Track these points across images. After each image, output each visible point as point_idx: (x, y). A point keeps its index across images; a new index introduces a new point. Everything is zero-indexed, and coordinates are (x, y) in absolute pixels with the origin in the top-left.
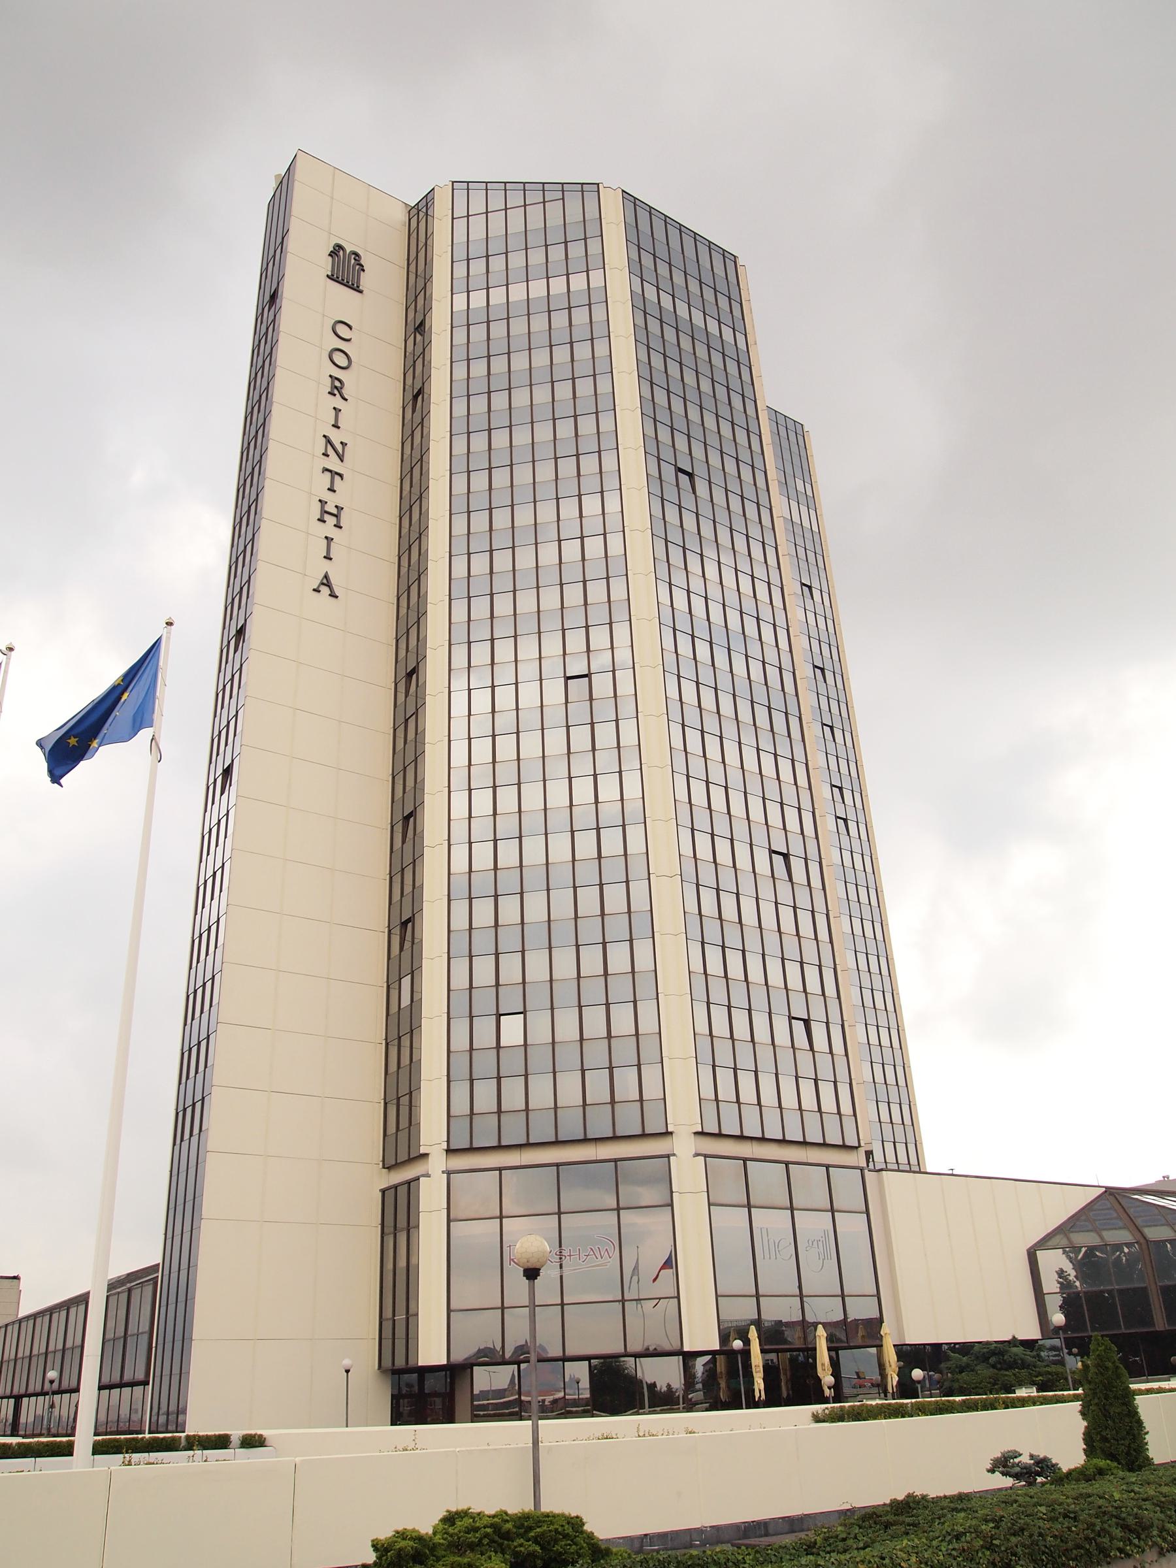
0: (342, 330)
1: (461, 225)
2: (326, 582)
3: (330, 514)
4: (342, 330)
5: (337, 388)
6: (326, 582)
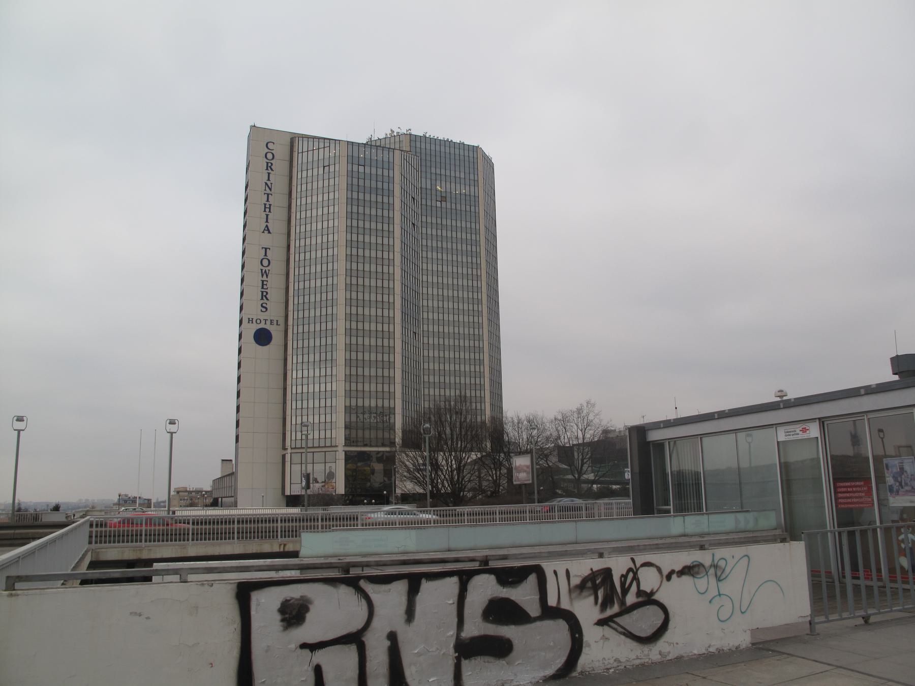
1: (300, 155)
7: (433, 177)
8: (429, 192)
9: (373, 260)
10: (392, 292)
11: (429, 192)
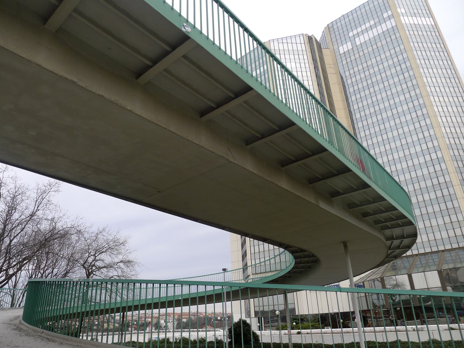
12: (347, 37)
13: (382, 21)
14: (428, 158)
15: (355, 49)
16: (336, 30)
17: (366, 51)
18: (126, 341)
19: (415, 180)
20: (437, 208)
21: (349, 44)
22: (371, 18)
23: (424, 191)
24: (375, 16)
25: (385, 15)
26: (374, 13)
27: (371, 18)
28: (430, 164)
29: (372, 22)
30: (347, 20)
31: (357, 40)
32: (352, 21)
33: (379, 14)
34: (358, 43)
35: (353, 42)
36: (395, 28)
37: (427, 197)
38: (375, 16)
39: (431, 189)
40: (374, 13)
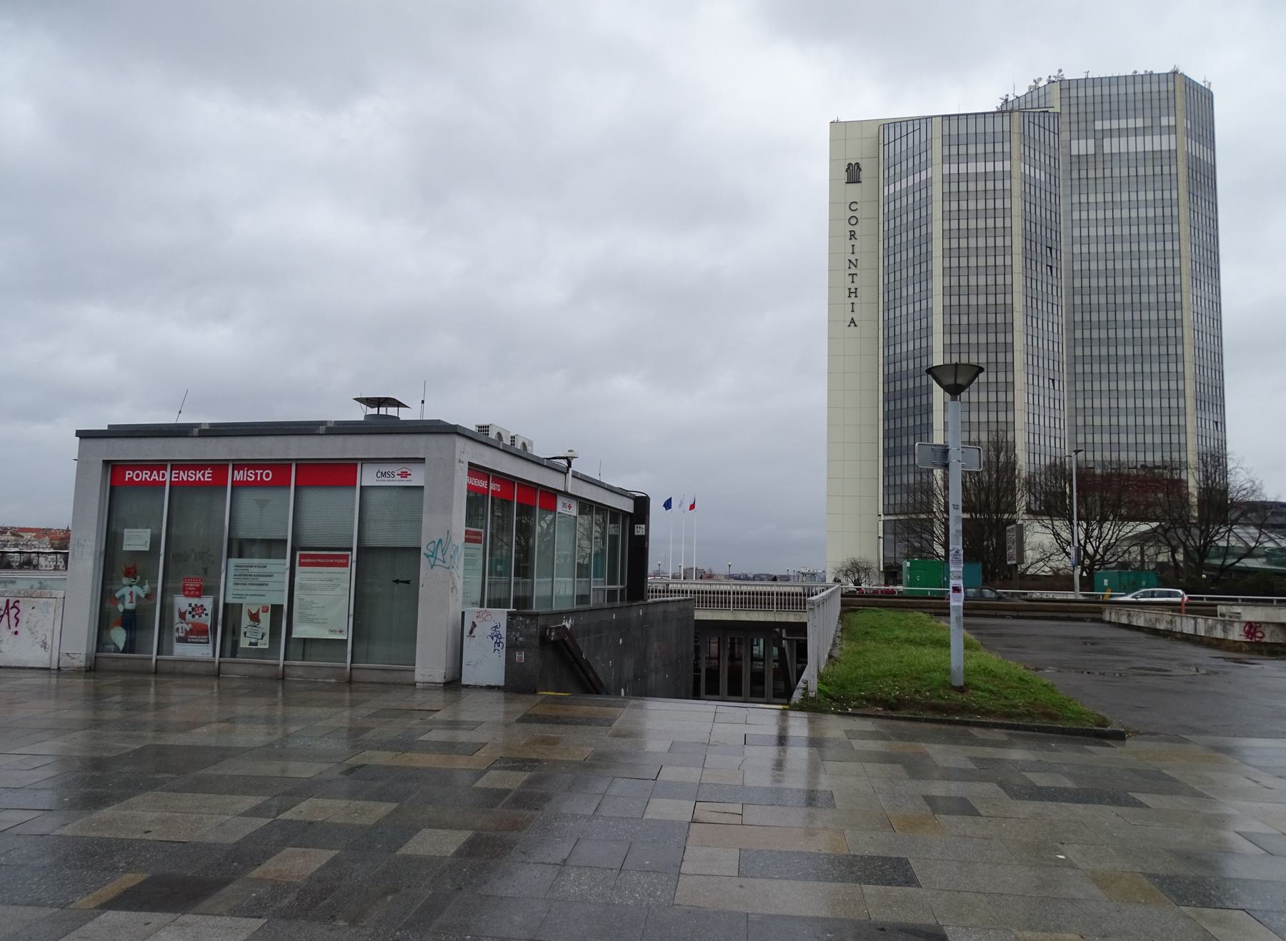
0: (854, 207)
2: (853, 321)
3: (853, 293)
4: (854, 207)
5: (853, 235)
6: (853, 321)
7: (1099, 135)
8: (1091, 159)
9: (982, 270)
10: (1008, 251)
11: (1091, 159)
12: (1090, 126)
13: (1156, 130)
14: (1163, 332)
15: (1100, 158)
16: (1074, 101)
17: (1116, 173)
18: (648, 816)
19: (1134, 239)
20: (1156, 403)
21: (1091, 142)
22: (1139, 113)
23: (1148, 412)
24: (1148, 112)
25: (1164, 122)
26: (1147, 105)
27: (1139, 113)
28: (1165, 394)
29: (1140, 123)
30: (1098, 90)
31: (1107, 141)
32: (1106, 99)
33: (1156, 112)
34: (1107, 150)
35: (1099, 143)
36: (1173, 154)
37: (1148, 421)
38: (1148, 112)
39: (1156, 394)
40: (1147, 105)
